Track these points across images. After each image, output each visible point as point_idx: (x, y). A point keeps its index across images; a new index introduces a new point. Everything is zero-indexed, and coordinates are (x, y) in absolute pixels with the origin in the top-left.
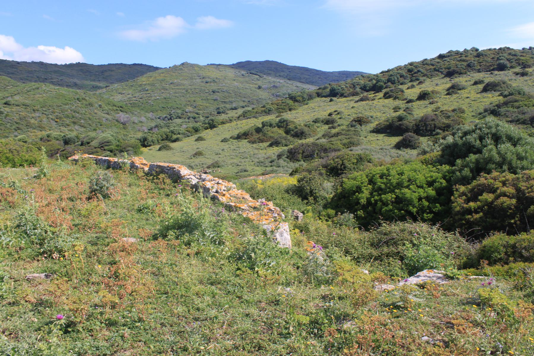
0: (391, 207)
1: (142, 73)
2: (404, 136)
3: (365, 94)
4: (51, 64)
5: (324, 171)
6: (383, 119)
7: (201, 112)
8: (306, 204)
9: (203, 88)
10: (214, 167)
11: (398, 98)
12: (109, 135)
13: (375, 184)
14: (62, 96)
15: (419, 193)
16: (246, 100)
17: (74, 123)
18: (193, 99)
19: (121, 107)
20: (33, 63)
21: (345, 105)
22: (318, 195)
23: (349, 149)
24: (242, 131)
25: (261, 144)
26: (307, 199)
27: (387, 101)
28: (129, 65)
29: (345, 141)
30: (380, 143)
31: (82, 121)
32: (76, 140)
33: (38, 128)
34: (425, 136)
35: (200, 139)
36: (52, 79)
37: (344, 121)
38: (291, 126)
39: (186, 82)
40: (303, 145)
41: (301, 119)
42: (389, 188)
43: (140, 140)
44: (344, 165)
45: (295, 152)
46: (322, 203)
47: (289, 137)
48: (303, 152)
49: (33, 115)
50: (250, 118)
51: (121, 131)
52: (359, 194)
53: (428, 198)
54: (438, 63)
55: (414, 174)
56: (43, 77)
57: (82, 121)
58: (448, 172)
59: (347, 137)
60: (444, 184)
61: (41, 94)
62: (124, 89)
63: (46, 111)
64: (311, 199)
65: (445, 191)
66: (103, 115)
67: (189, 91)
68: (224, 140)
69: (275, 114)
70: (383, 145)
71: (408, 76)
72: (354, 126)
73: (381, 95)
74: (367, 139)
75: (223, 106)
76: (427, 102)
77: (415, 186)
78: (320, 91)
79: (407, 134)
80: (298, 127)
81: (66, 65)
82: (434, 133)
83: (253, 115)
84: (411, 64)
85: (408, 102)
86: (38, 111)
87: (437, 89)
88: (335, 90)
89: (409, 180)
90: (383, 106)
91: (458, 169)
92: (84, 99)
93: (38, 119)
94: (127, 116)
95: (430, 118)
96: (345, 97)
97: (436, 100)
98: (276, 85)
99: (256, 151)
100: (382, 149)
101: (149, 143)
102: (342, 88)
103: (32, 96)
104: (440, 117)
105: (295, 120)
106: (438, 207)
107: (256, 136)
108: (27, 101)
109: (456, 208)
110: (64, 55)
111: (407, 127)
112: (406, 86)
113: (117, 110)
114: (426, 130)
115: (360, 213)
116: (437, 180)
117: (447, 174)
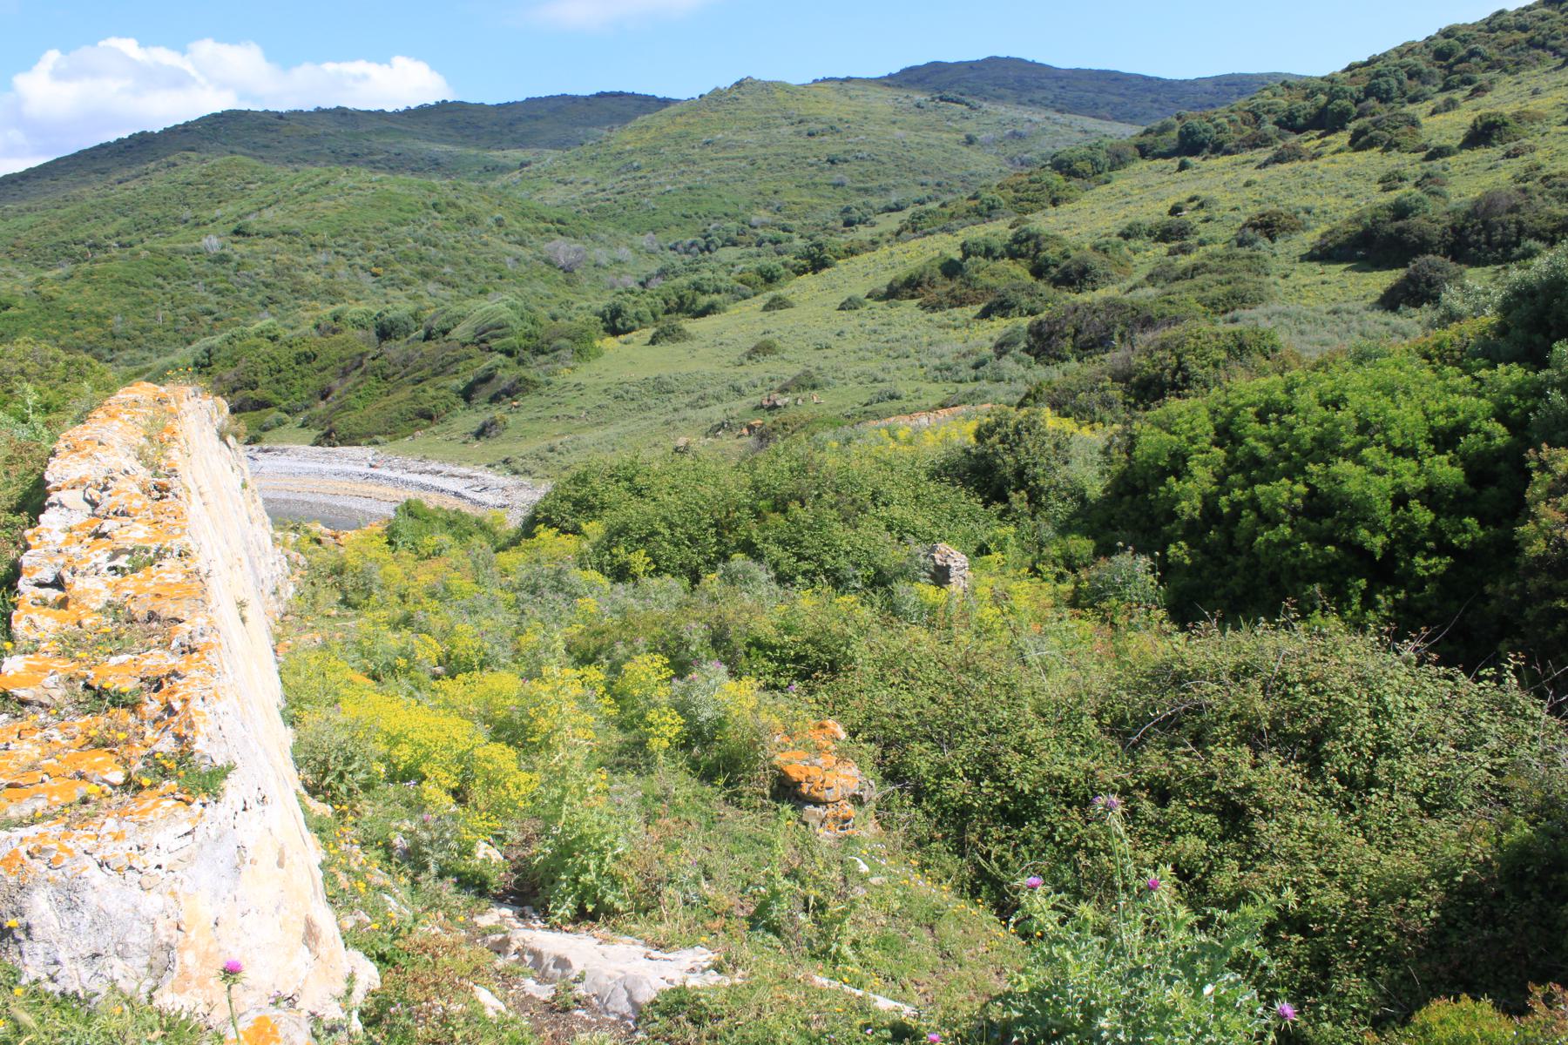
0: (1288, 531)
1: (624, 119)
2: (1412, 265)
3: (1293, 139)
4: (369, 112)
5: (1116, 393)
6: (1346, 214)
7: (796, 223)
8: (1000, 517)
9: (800, 152)
10: (802, 387)
11: (1397, 145)
12: (502, 305)
13: (1238, 440)
14: (389, 199)
15: (1395, 475)
16: (930, 180)
17: (425, 275)
18: (772, 186)
19: (560, 221)
20: (319, 111)
21: (1226, 177)
22: (1042, 483)
23: (1228, 316)
24: (902, 273)
25: (956, 312)
26: (1005, 499)
27: (1360, 157)
28: (586, 98)
29: (1217, 292)
30: (1331, 292)
31: (447, 269)
32: (414, 324)
33: (323, 297)
34: (1486, 264)
35: (777, 304)
36: (371, 153)
37: (1218, 227)
38: (1051, 253)
39: (747, 137)
40: (1076, 310)
41: (1084, 229)
42: (1288, 458)
43: (603, 315)
44: (1185, 369)
45: (1052, 333)
46: (1061, 509)
47: (1042, 286)
48: (1078, 331)
49: (311, 260)
50: (930, 234)
51: (560, 292)
52: (1178, 479)
53: (1432, 496)
54: (1543, 19)
55: (1384, 401)
56: (347, 150)
57: (447, 269)
58: (1520, 391)
59: (1224, 278)
60: (1499, 441)
61: (334, 199)
62: (573, 169)
63: (345, 246)
64: (1018, 500)
65: (1503, 466)
66: (508, 247)
67: (760, 162)
68: (849, 305)
69: (1009, 216)
70: (1343, 298)
71: (1437, 71)
72: (1251, 243)
73: (1343, 138)
74: (1290, 282)
75: (860, 201)
76: (1496, 152)
77: (1383, 448)
78: (1149, 139)
79: (1421, 259)
80: (1072, 253)
81: (408, 111)
82: (1516, 251)
83: (942, 223)
84: (1448, 33)
85: (1431, 157)
86: (324, 246)
87: (1534, 105)
88: (1194, 133)
89: (1364, 427)
90: (1347, 175)
91: (1558, 379)
92: (454, 205)
93: (325, 271)
94: (577, 246)
95: (1505, 202)
96: (1228, 152)
97: (1527, 142)
98: (1019, 129)
99: (938, 335)
100: (1335, 312)
101: (629, 324)
102: (1217, 126)
103: (309, 206)
104: (1539, 199)
105: (1066, 235)
106: (1472, 530)
107: (944, 287)
108: (294, 222)
109: (1530, 543)
110: (400, 83)
111: (1422, 238)
112: (1428, 106)
113: (548, 231)
114: (1489, 242)
115: (1178, 551)
116: (1473, 426)
117: (1513, 399)
